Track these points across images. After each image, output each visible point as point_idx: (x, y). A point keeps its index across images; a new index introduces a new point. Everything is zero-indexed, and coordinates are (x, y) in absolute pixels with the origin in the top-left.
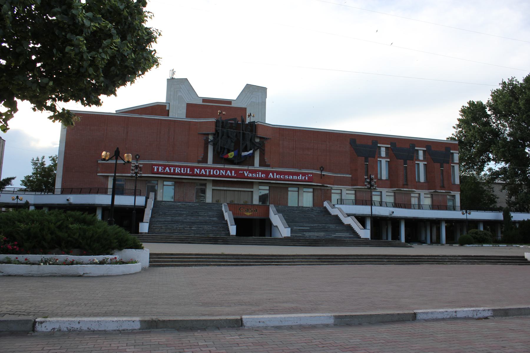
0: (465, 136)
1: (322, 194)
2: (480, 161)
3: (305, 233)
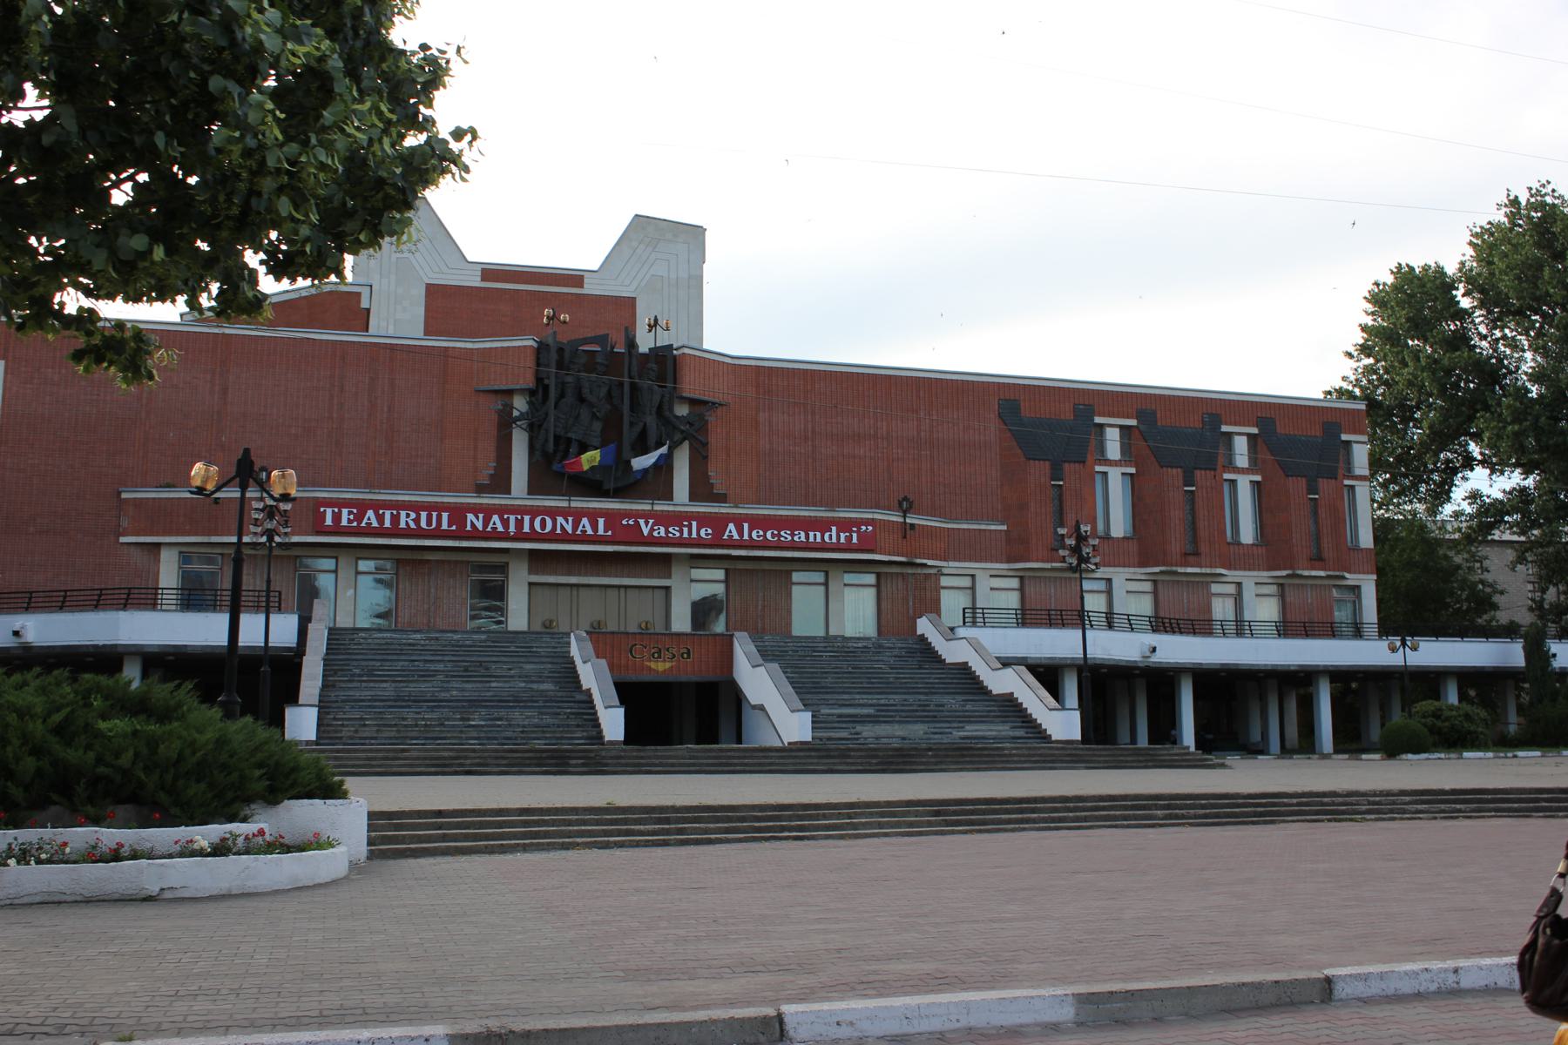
0: (1386, 383)
1: (908, 592)
2: (1437, 470)
3: (859, 728)
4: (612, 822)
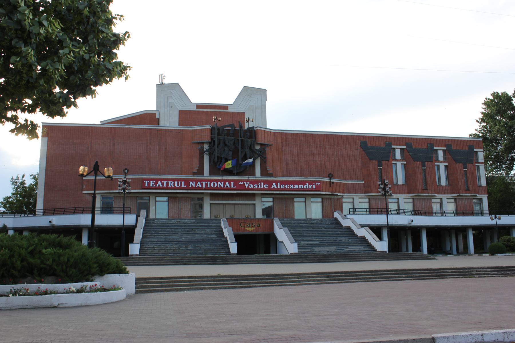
0: (490, 132)
1: (332, 203)
3: (314, 248)
4: (219, 281)
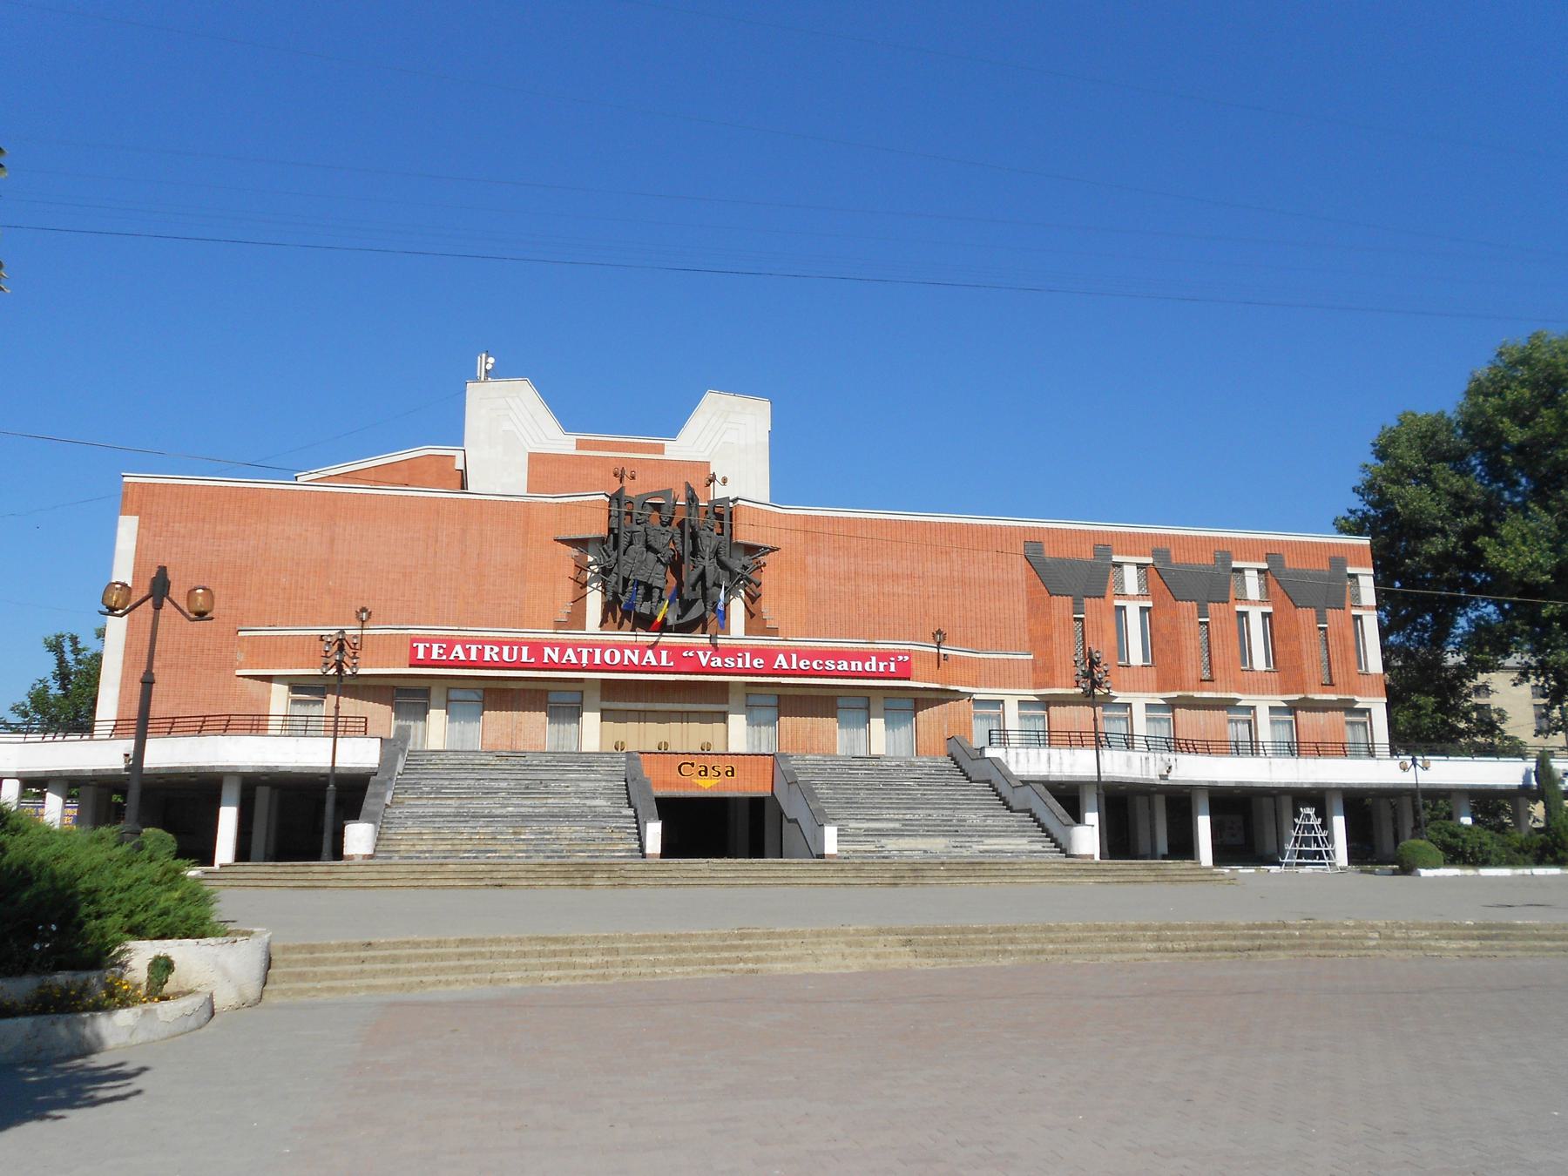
3: (884, 841)
